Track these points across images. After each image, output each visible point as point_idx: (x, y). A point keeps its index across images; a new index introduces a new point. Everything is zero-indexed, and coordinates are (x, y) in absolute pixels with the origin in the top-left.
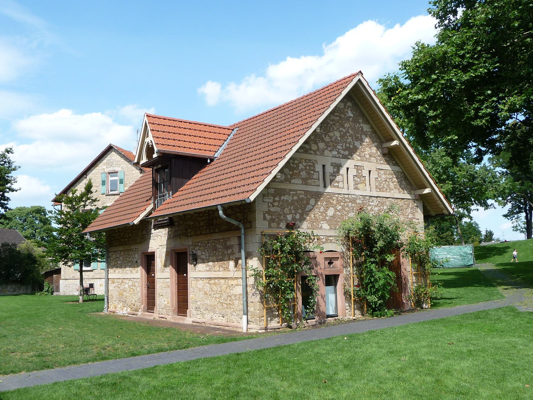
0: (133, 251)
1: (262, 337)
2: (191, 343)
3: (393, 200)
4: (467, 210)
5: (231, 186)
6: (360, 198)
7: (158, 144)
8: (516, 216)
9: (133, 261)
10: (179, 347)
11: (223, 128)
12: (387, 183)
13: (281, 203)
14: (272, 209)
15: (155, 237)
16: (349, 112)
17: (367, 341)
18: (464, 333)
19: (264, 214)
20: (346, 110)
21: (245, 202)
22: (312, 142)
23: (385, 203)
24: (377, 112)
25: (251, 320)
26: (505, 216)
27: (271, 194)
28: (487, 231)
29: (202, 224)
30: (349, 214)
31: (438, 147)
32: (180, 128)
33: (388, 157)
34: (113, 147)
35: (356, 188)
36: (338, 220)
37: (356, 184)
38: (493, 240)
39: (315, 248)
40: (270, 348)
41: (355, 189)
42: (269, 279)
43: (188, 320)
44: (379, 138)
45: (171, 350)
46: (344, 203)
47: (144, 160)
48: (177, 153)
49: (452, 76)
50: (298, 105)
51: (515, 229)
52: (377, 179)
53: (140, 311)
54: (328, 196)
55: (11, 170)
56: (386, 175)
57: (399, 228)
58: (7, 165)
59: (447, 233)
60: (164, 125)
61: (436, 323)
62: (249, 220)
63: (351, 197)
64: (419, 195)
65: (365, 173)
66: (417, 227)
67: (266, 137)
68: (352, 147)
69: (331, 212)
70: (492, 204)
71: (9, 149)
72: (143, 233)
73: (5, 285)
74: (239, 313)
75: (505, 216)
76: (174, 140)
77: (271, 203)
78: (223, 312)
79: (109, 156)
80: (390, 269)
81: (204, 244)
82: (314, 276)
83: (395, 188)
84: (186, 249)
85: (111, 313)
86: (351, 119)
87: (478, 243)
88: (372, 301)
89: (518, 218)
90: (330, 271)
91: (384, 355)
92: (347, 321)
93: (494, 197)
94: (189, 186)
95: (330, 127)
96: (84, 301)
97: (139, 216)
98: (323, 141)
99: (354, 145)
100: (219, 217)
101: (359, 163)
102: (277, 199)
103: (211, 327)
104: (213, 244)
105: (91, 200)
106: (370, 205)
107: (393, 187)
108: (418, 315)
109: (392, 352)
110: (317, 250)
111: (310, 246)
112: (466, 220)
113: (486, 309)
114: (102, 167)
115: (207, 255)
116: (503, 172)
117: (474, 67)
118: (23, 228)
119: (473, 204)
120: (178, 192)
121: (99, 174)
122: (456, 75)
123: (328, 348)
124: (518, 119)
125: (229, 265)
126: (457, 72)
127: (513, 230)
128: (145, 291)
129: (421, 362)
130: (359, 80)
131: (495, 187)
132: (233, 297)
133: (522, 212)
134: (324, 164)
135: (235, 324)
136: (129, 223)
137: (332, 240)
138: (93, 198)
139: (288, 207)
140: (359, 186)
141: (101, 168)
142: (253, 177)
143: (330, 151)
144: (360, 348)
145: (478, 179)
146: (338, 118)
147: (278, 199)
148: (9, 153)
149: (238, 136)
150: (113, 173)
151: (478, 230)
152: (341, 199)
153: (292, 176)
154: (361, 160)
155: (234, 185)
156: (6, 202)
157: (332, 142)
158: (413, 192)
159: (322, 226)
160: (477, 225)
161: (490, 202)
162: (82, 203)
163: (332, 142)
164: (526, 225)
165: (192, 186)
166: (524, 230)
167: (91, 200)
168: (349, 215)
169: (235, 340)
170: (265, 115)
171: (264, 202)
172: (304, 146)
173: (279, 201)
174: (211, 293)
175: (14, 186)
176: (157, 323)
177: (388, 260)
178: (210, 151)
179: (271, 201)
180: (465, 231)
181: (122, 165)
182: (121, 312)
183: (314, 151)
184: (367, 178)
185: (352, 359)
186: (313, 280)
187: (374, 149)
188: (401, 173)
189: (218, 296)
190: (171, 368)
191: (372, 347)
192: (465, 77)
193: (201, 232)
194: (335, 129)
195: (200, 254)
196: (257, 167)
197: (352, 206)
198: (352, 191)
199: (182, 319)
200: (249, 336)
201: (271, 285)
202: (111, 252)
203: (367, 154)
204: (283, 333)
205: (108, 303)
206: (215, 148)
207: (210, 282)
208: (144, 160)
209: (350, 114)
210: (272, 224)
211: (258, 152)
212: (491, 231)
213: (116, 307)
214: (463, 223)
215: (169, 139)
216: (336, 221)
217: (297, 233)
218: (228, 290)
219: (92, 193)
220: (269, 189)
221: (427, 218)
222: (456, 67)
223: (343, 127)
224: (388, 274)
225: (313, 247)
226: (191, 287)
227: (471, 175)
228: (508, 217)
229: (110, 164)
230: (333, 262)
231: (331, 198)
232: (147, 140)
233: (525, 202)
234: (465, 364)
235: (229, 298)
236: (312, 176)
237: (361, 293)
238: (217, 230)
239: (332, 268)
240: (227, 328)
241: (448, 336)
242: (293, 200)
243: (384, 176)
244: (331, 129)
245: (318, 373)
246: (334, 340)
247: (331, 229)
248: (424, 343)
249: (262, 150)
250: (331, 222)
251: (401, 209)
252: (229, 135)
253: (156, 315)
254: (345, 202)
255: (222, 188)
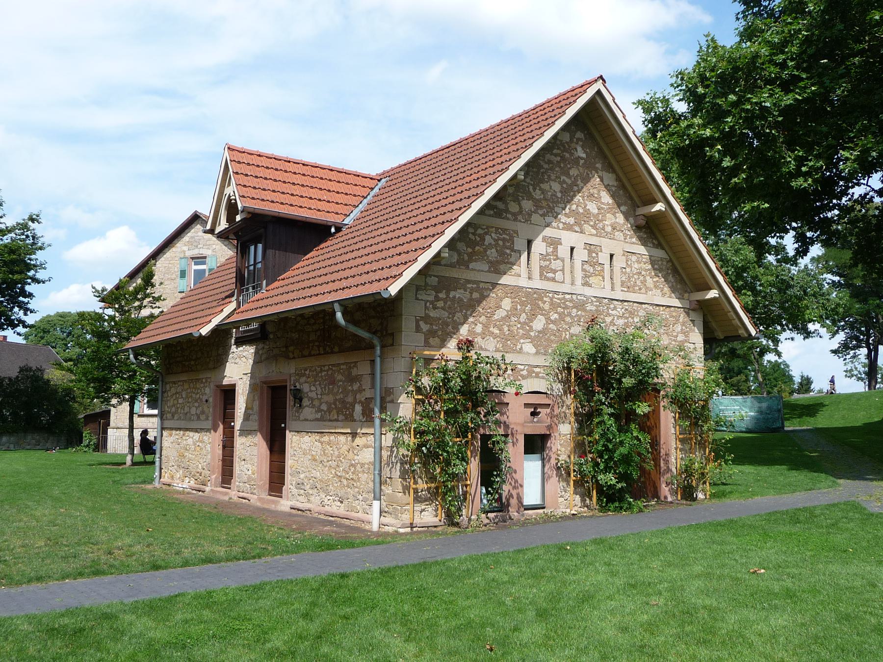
0: (202, 382)
1: (402, 541)
2: (270, 548)
3: (651, 308)
4: (773, 341)
5: (362, 269)
6: (592, 301)
7: (243, 197)
8: (852, 352)
9: (201, 400)
10: (245, 556)
11: (363, 177)
12: (642, 278)
13: (449, 303)
14: (433, 314)
15: (238, 360)
16: (579, 149)
17: (589, 558)
18: (771, 552)
19: (417, 322)
20: (573, 145)
21: (380, 297)
22: (509, 199)
23: (636, 313)
24: (625, 145)
25: (386, 509)
26: (835, 352)
27: (431, 286)
28: (802, 377)
29: (313, 337)
30: (572, 328)
31: (730, 235)
32: (286, 171)
33: (645, 233)
34: (199, 217)
35: (586, 284)
36: (552, 338)
37: (586, 275)
38: (812, 391)
39: (506, 385)
40: (407, 566)
41: (583, 285)
42: (421, 438)
43: (284, 504)
44: (631, 198)
45: (228, 560)
46: (563, 308)
47: (223, 225)
48: (277, 214)
49: (766, 98)
50: (492, 136)
51: (849, 374)
52: (624, 270)
53: (209, 485)
54: (535, 296)
55: (36, 249)
56: (640, 263)
57: (660, 356)
58: (31, 241)
59: (739, 377)
60: (258, 166)
61: (719, 528)
62: (389, 332)
63: (577, 299)
64: (697, 301)
65: (604, 258)
66: (692, 356)
67: (430, 189)
68: (581, 211)
69: (539, 323)
70: (816, 330)
71: (34, 217)
72: (219, 352)
73: (23, 434)
74: (367, 496)
75: (835, 352)
76: (274, 191)
77: (432, 303)
78: (341, 493)
79: (193, 231)
80: (642, 429)
81: (315, 373)
82: (502, 435)
83: (656, 287)
84: (286, 381)
85: (164, 487)
86: (582, 162)
87: (787, 394)
88: (606, 483)
89: (854, 357)
90: (537, 428)
91: (619, 591)
92: (560, 517)
93: (821, 319)
94: (297, 272)
95: (543, 173)
96: (134, 464)
97: (210, 321)
98: (530, 197)
99: (585, 207)
100: (337, 326)
101: (594, 240)
102: (442, 295)
103: (320, 519)
104: (330, 373)
105: (151, 299)
106: (609, 315)
107: (652, 286)
108: (685, 512)
109: (634, 586)
110: (511, 390)
111: (497, 383)
112: (770, 357)
113: (808, 505)
114: (181, 247)
115: (319, 393)
116: (833, 281)
117: (802, 84)
118: (66, 345)
119: (784, 330)
120: (276, 282)
121: (177, 259)
122: (771, 96)
123: (513, 569)
124: (870, 186)
125: (353, 411)
126: (773, 91)
127: (846, 376)
128: (219, 451)
129: (689, 613)
130: (599, 92)
131: (823, 303)
132: (358, 467)
133: (863, 347)
134: (530, 238)
135: (360, 515)
136: (191, 333)
137: (540, 373)
138: (156, 295)
139: (461, 311)
140: (592, 280)
141: (179, 250)
142: (400, 254)
143: (541, 215)
144: (575, 574)
145: (795, 288)
146: (559, 159)
147: (445, 297)
148: (33, 223)
149: (387, 189)
150: (198, 258)
151: (789, 374)
152: (559, 301)
153: (471, 255)
154: (596, 235)
155: (367, 268)
156: (26, 300)
157: (546, 200)
158: (686, 295)
159: (522, 347)
160: (788, 366)
161: (811, 327)
162: (137, 304)
163: (546, 200)
164: (867, 369)
165: (302, 270)
166: (863, 376)
167: (151, 299)
168: (571, 331)
169: (352, 546)
170: (435, 155)
171: (417, 299)
172: (494, 203)
173: (445, 301)
174: (322, 459)
175: (40, 275)
176: (231, 508)
177: (639, 411)
178: (337, 213)
179: (431, 298)
180: (767, 375)
181: (214, 246)
182: (180, 485)
183: (514, 214)
184: (607, 267)
185: (554, 598)
186: (500, 442)
187: (620, 219)
188: (668, 262)
189: (334, 464)
190: (206, 600)
191: (598, 572)
192: (788, 100)
193: (310, 352)
194: (553, 177)
195: (308, 390)
196: (409, 238)
197: (577, 315)
198: (579, 289)
199: (273, 502)
200: (382, 538)
201: (424, 448)
202: (169, 382)
203: (607, 225)
204: (441, 535)
205: (161, 469)
206: (346, 210)
207: (322, 440)
208: (223, 225)
209: (581, 153)
210: (431, 340)
211: (415, 213)
212: (809, 377)
213: (172, 477)
214: (766, 362)
215: (264, 190)
216: (548, 340)
217: (475, 357)
218: (351, 455)
219: (153, 286)
220: (428, 278)
221: (709, 340)
222: (770, 82)
223: (568, 175)
224: (637, 438)
225: (503, 384)
226: (291, 447)
227: (783, 281)
228: (840, 355)
229: (193, 244)
230: (539, 413)
231: (541, 299)
232: (228, 191)
233: (868, 331)
234: (779, 620)
235: (352, 469)
236: (508, 259)
237: (587, 468)
238: (336, 349)
239: (537, 422)
240: (347, 522)
241: (741, 556)
242: (471, 299)
243: (636, 266)
244: (546, 177)
245: (483, 626)
246: (529, 555)
247: (537, 353)
248: (698, 569)
249: (422, 210)
250: (540, 340)
251: (664, 324)
252: (372, 189)
253: (234, 492)
254: (566, 307)
255: (348, 273)
